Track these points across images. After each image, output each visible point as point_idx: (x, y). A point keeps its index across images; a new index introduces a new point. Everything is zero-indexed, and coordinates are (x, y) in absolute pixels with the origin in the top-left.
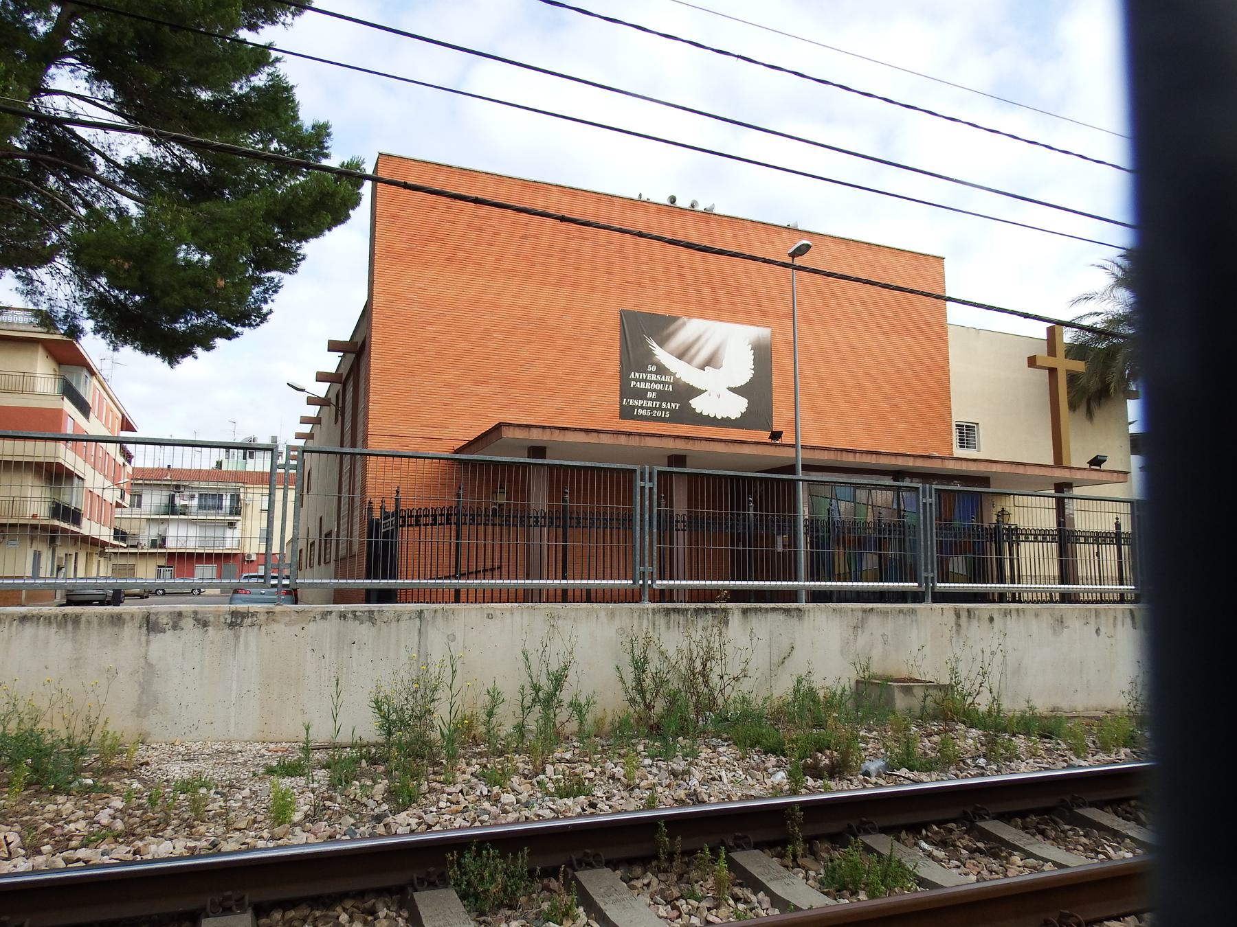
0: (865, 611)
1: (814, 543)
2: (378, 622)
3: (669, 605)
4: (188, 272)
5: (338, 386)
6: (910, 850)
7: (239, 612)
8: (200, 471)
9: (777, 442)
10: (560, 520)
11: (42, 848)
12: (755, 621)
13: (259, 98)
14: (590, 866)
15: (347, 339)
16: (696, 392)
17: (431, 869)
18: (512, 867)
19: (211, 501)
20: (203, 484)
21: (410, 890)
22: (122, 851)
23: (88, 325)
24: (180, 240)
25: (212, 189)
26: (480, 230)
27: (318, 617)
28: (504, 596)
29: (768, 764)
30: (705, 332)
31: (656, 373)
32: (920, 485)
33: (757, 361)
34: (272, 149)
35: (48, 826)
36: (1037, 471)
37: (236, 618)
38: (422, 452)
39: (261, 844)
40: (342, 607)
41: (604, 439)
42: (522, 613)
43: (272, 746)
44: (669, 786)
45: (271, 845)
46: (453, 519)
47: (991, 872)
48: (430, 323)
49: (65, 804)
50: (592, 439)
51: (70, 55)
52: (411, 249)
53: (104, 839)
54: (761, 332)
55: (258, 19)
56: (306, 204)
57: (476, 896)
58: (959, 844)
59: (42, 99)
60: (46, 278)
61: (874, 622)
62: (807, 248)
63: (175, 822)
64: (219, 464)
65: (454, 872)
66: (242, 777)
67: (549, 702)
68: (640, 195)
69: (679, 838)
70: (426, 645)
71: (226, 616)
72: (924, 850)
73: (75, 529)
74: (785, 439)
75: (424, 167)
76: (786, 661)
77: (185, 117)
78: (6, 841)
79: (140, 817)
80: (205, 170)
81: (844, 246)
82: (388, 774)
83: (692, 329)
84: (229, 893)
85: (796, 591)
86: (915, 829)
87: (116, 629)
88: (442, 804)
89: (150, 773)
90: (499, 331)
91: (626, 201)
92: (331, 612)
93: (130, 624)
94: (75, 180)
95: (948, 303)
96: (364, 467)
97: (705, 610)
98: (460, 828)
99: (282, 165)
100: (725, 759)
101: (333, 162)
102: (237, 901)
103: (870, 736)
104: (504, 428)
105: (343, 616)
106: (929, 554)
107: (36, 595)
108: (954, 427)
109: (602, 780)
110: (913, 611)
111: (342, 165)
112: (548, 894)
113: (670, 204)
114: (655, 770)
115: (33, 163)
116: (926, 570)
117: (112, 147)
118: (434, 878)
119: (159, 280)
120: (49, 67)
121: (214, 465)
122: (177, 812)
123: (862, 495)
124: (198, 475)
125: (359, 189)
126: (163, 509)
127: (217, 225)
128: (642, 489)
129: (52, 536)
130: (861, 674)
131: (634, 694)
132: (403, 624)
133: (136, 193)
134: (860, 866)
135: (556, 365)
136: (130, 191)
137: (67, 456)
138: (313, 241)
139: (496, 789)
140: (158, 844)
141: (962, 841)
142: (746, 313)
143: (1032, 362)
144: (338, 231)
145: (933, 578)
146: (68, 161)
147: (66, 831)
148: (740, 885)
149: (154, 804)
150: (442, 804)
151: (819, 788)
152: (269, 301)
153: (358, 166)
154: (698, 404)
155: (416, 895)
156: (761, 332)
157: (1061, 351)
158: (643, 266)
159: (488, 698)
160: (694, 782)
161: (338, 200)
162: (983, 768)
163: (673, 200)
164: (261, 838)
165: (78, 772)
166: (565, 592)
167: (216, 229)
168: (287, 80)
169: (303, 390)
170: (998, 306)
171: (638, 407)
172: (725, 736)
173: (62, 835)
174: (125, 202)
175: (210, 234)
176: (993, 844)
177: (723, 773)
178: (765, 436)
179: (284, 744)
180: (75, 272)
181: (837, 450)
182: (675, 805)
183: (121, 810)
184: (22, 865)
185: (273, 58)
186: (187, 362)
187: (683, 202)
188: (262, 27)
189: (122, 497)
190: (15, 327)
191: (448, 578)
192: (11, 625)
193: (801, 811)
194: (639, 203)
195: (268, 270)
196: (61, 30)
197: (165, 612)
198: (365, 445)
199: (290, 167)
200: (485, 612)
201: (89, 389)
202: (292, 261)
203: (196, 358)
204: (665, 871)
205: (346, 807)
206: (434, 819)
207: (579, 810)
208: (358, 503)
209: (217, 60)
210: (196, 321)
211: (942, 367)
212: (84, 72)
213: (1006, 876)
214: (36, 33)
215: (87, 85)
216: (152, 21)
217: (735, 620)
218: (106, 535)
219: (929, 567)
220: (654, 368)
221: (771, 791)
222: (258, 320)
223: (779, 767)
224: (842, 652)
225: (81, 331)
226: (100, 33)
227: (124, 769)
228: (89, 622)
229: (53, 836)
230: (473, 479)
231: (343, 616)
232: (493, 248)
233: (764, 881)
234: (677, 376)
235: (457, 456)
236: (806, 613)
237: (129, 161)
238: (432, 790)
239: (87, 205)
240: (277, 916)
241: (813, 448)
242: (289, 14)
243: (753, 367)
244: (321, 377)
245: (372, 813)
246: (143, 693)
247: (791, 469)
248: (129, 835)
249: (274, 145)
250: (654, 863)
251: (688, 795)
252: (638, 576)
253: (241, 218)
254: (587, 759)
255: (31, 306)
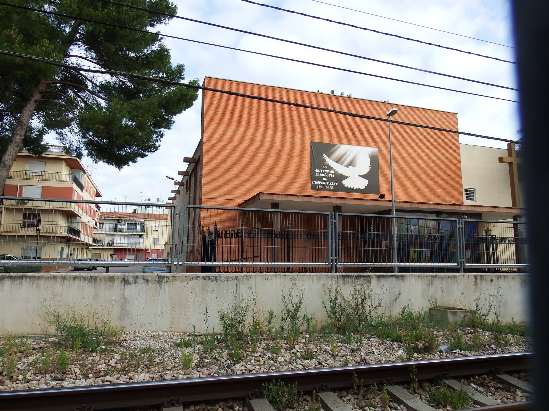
0: (433, 277)
1: (400, 245)
2: (219, 281)
3: (344, 274)
4: (127, 130)
5: (187, 177)
6: (467, 387)
7: (161, 276)
8: (160, 214)
9: (383, 199)
10: (287, 236)
11: (89, 375)
12: (383, 281)
13: (155, 55)
14: (324, 390)
15: (191, 157)
16: (346, 177)
17: (257, 390)
18: (290, 390)
19: (132, 226)
20: (128, 219)
21: (247, 399)
22: (124, 378)
23: (85, 152)
24: (124, 116)
25: (136, 94)
26: (249, 108)
27: (194, 279)
28: (276, 270)
29: (395, 347)
30: (348, 151)
31: (327, 169)
32: (457, 219)
33: (372, 163)
34: (160, 76)
35: (90, 366)
36: (505, 211)
37: (160, 279)
38: (225, 207)
39: (181, 376)
40: (204, 274)
41: (305, 199)
42: (280, 278)
43: (175, 334)
44: (352, 355)
45: (185, 377)
46: (240, 235)
47: (507, 398)
48: (228, 150)
49: (96, 357)
50: (300, 199)
51: (79, 40)
52: (219, 117)
53: (114, 372)
54: (373, 150)
55: (154, 22)
56: (175, 99)
57: (276, 402)
58: (490, 385)
59: (67, 59)
60: (69, 133)
61: (437, 282)
62: (395, 112)
63: (142, 366)
64: (135, 211)
65: (266, 392)
66: (166, 347)
67: (294, 317)
68: (318, 90)
69: (363, 379)
70: (239, 292)
71: (156, 278)
72: (473, 388)
73: (78, 238)
74: (386, 198)
75: (224, 82)
76: (397, 299)
77: (125, 64)
78: (75, 372)
79: (127, 363)
80: (133, 86)
81: (411, 110)
82: (227, 347)
83: (342, 149)
84: (173, 397)
85: (393, 268)
86: (468, 378)
87: (111, 283)
88: (253, 361)
89: (127, 344)
90: (258, 152)
91: (312, 93)
92: (199, 277)
93: (117, 281)
94: (80, 92)
95: (460, 135)
96: (200, 212)
97: (361, 276)
98: (264, 372)
99: (165, 84)
100: (375, 344)
101: (185, 81)
102: (176, 401)
103: (439, 334)
104: (261, 195)
105: (204, 278)
106: (462, 250)
107: (61, 267)
108: (464, 191)
109: (321, 352)
110: (455, 277)
111: (190, 82)
112: (306, 402)
113: (331, 94)
114: (344, 348)
115: (63, 85)
116: (461, 258)
117: (95, 78)
118: (258, 394)
119: (115, 133)
120: (70, 46)
121: (133, 211)
122: (142, 361)
123: (422, 223)
124: (126, 215)
125: (197, 92)
126: (112, 230)
127: (138, 109)
128: (332, 222)
129: (68, 241)
130: (433, 305)
131: (330, 314)
132: (229, 282)
133: (104, 97)
134: (447, 394)
135: (282, 167)
136: (102, 96)
137: (75, 208)
138: (178, 115)
139: (275, 355)
140: (139, 375)
141: (491, 384)
142: (367, 141)
143: (501, 160)
144: (188, 110)
145: (464, 262)
146: (77, 84)
147: (98, 368)
148: (391, 401)
149: (132, 358)
150: (253, 361)
151: (420, 358)
152: (159, 141)
153: (196, 82)
154: (346, 183)
155: (251, 401)
156: (373, 150)
157: (514, 154)
158: (321, 122)
159: (269, 315)
160: (363, 354)
161: (188, 97)
162: (495, 350)
163: (333, 92)
164: (180, 374)
165: (98, 343)
166: (289, 268)
167: (138, 111)
168: (167, 47)
169: (173, 179)
170: (488, 136)
171: (319, 185)
172: (372, 333)
173: (97, 370)
174: (100, 100)
175: (135, 113)
176: (505, 386)
177: (375, 350)
178: (377, 197)
179: (180, 333)
180: (80, 131)
181: (410, 202)
182: (356, 364)
183: (119, 360)
184: (85, 383)
185: (160, 38)
186: (126, 167)
187: (337, 93)
188: (156, 25)
189: (96, 225)
190: (54, 153)
191: (235, 261)
192: (70, 280)
193: (416, 368)
194: (318, 94)
195: (159, 128)
196: (75, 30)
197: (131, 276)
198: (200, 204)
199: (166, 84)
200: (264, 277)
201: (83, 179)
202: (169, 124)
203: (129, 166)
204: (357, 394)
205: (212, 361)
206: (252, 368)
207: (314, 366)
208: (197, 228)
209: (137, 40)
210: (129, 150)
211: (457, 163)
212: (84, 47)
213: (516, 402)
214: (65, 32)
215: (85, 52)
216: (112, 25)
217: (374, 281)
218: (90, 241)
219: (462, 257)
220: (326, 167)
221: (398, 359)
222: (154, 149)
223: (399, 348)
224: (423, 296)
225: (82, 155)
226: (91, 30)
227: (117, 342)
228: (101, 280)
229: (93, 370)
230: (246, 217)
231: (204, 278)
232: (254, 116)
233: (403, 400)
234: (336, 170)
235: (240, 208)
236: (406, 278)
237: (101, 84)
238: (247, 355)
239: (85, 102)
240: (192, 408)
241: (399, 202)
242: (167, 19)
243: (370, 166)
244: (180, 173)
245: (223, 364)
246: (122, 310)
247: (389, 212)
248: (124, 371)
249: (161, 75)
250: (351, 390)
251: (361, 360)
252: (330, 261)
253: (148, 106)
254: (312, 343)
255: (62, 145)
